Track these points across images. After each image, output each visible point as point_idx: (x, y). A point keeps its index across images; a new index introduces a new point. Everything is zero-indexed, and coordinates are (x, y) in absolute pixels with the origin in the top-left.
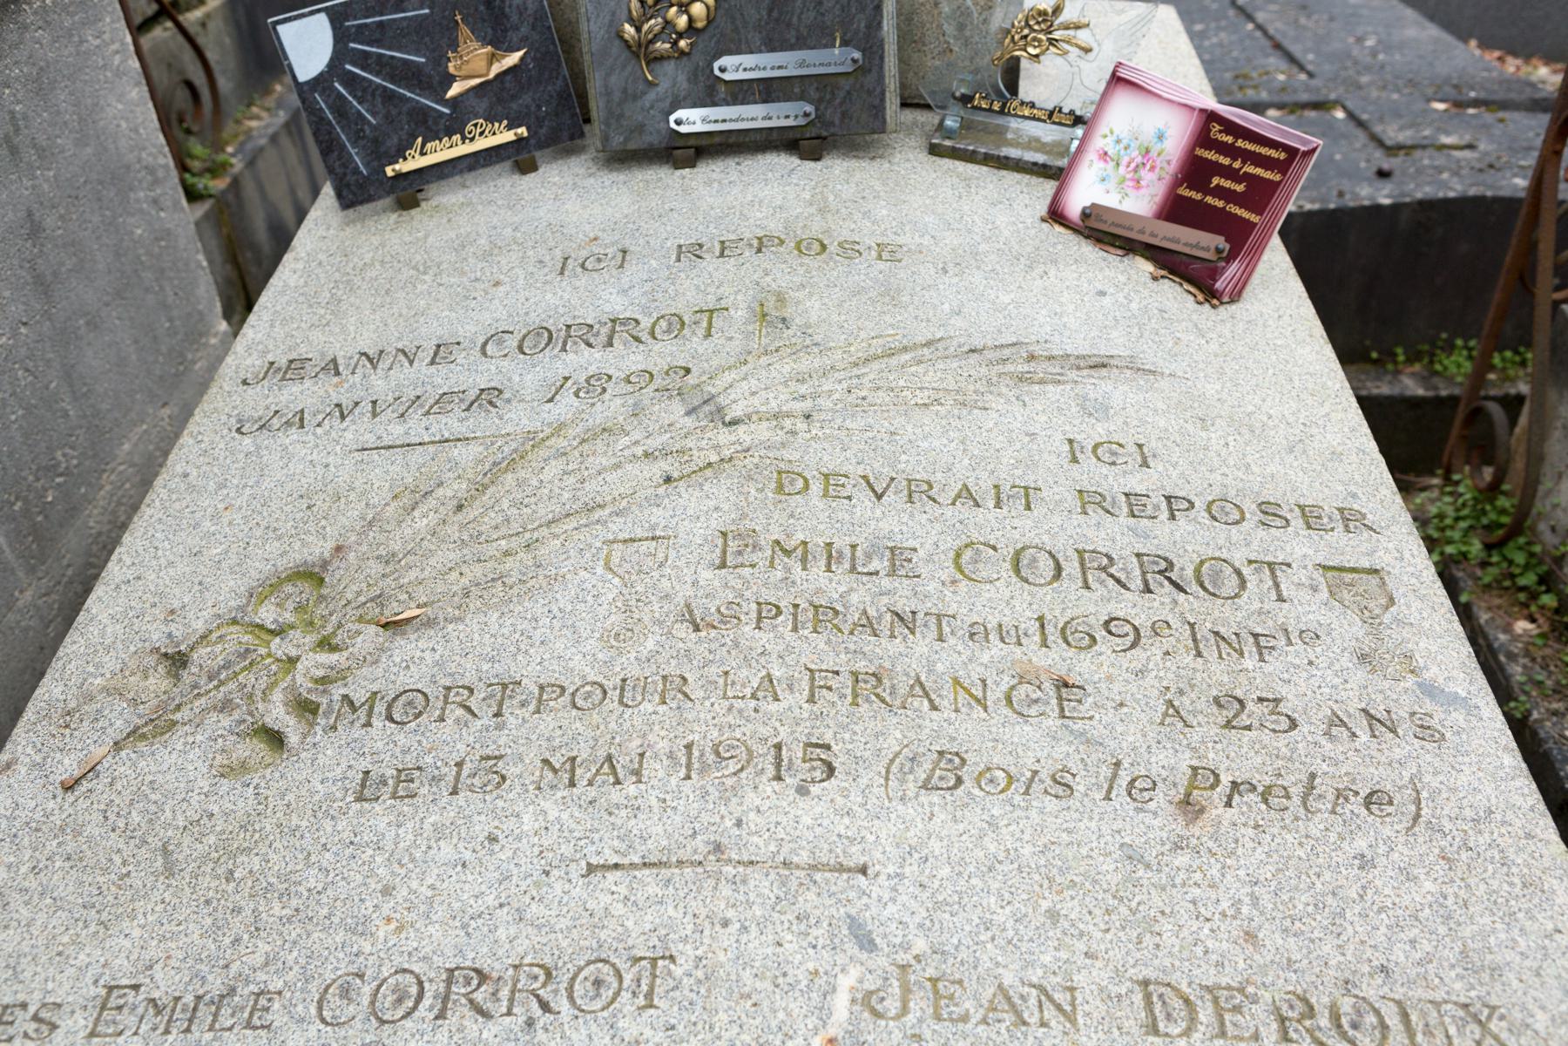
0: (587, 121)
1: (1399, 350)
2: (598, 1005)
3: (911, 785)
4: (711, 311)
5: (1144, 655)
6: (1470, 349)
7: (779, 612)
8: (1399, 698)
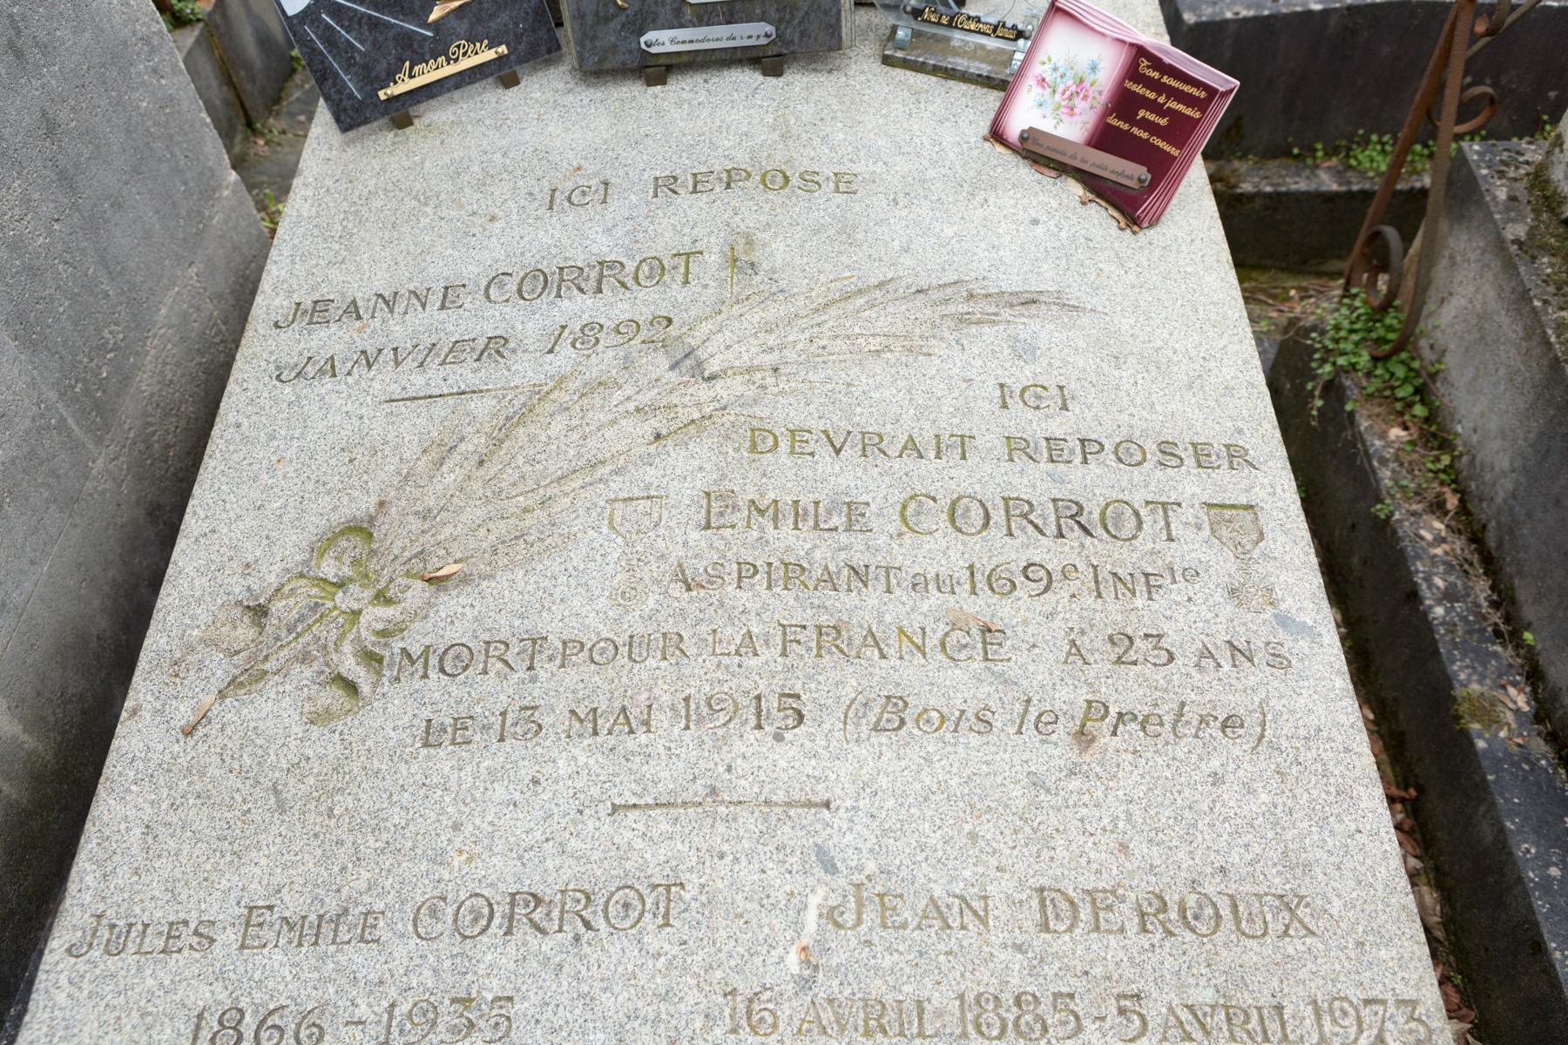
0: (560, 24)
1: (1319, 146)
2: (627, 924)
3: (864, 728)
4: (688, 255)
5: (1054, 599)
6: (1383, 144)
7: (756, 572)
8: (1257, 628)
